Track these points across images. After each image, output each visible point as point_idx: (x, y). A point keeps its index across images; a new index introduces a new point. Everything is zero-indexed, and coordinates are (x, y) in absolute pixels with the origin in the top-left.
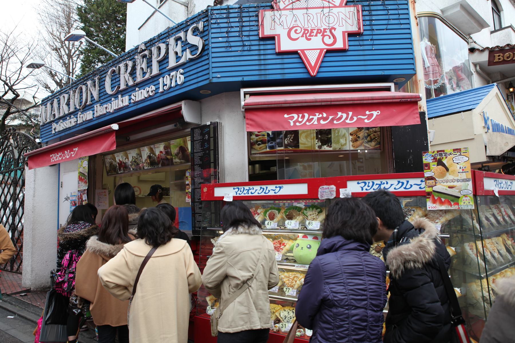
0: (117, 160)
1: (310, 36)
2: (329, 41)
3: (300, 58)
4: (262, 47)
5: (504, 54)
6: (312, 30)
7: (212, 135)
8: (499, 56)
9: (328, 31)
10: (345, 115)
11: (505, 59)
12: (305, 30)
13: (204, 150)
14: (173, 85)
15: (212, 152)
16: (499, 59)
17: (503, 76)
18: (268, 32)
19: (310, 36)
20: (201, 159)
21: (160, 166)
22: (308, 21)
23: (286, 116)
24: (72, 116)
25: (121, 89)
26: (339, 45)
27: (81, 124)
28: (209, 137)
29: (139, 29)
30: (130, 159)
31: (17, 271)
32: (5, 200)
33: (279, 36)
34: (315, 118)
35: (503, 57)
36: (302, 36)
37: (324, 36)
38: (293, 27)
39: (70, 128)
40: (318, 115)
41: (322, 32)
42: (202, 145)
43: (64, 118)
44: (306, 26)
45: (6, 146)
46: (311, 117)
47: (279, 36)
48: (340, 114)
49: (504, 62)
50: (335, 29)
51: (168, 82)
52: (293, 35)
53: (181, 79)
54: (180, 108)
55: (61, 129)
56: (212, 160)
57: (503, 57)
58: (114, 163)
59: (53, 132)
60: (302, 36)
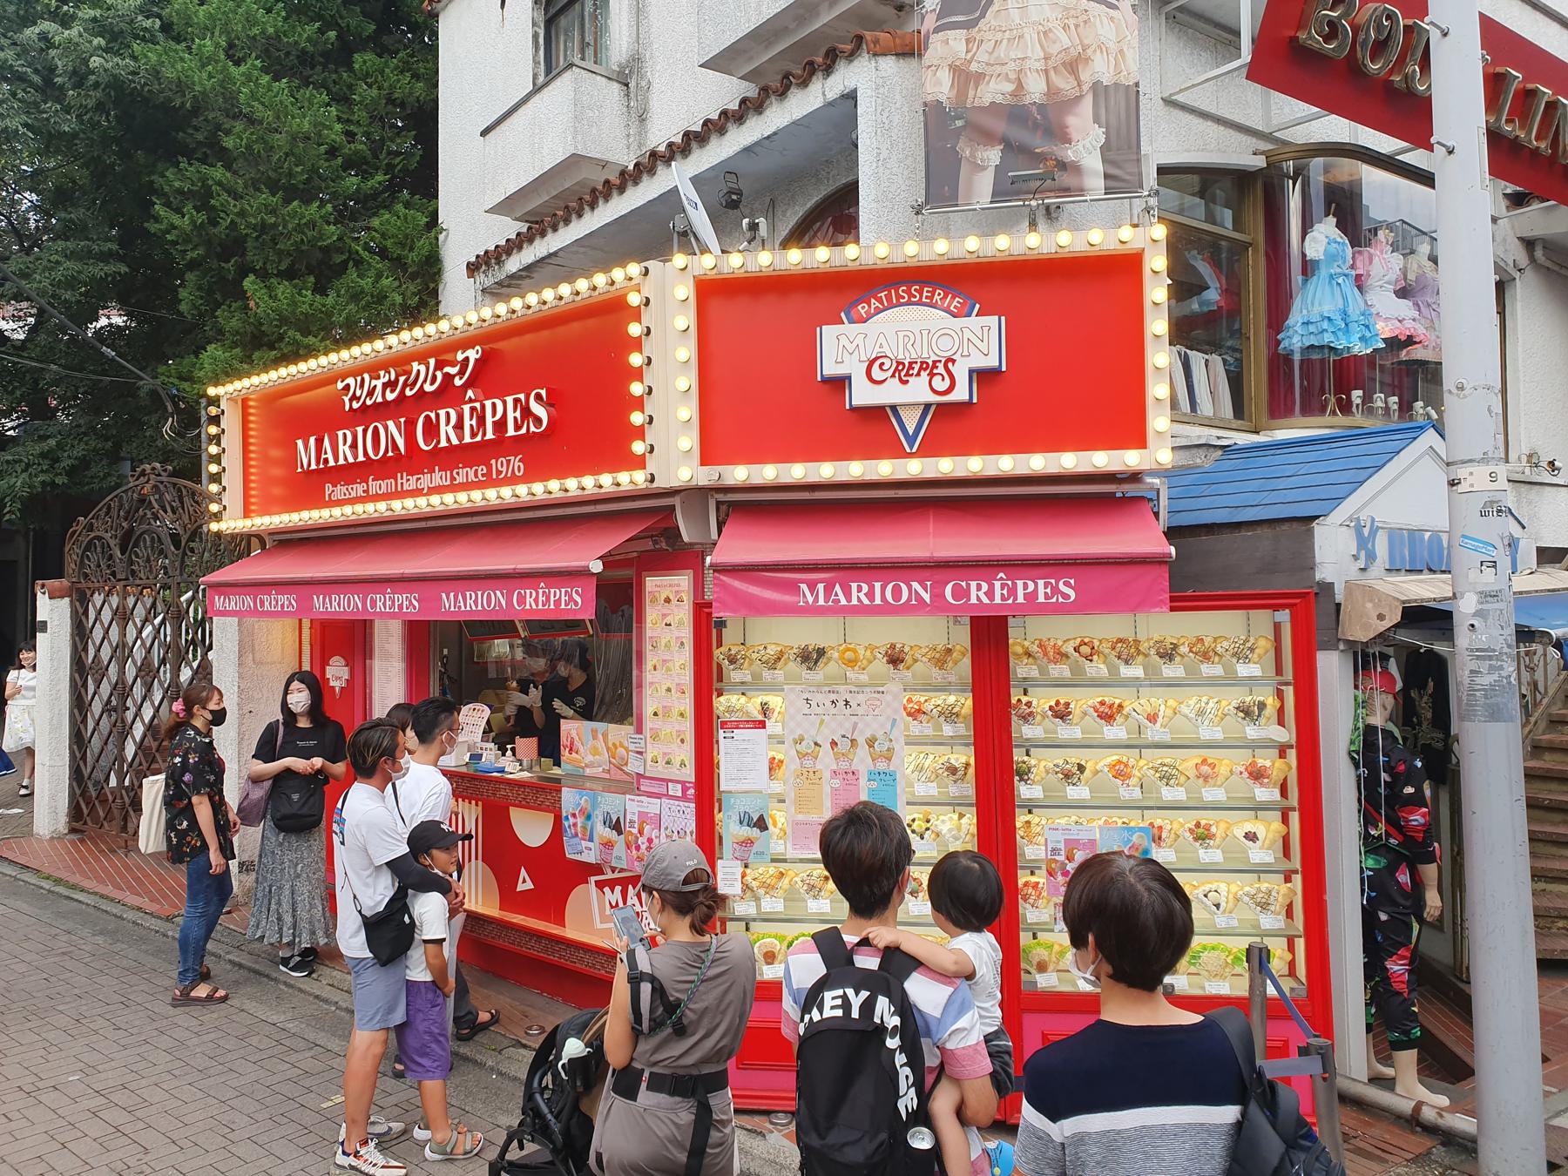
1: (907, 374)
9: (941, 366)
10: (423, 368)
12: (899, 363)
19: (907, 374)
22: (905, 346)
26: (961, 394)
29: (484, 133)
37: (932, 375)
38: (877, 358)
41: (929, 368)
44: (901, 357)
46: (374, 382)
50: (954, 361)
52: (877, 374)
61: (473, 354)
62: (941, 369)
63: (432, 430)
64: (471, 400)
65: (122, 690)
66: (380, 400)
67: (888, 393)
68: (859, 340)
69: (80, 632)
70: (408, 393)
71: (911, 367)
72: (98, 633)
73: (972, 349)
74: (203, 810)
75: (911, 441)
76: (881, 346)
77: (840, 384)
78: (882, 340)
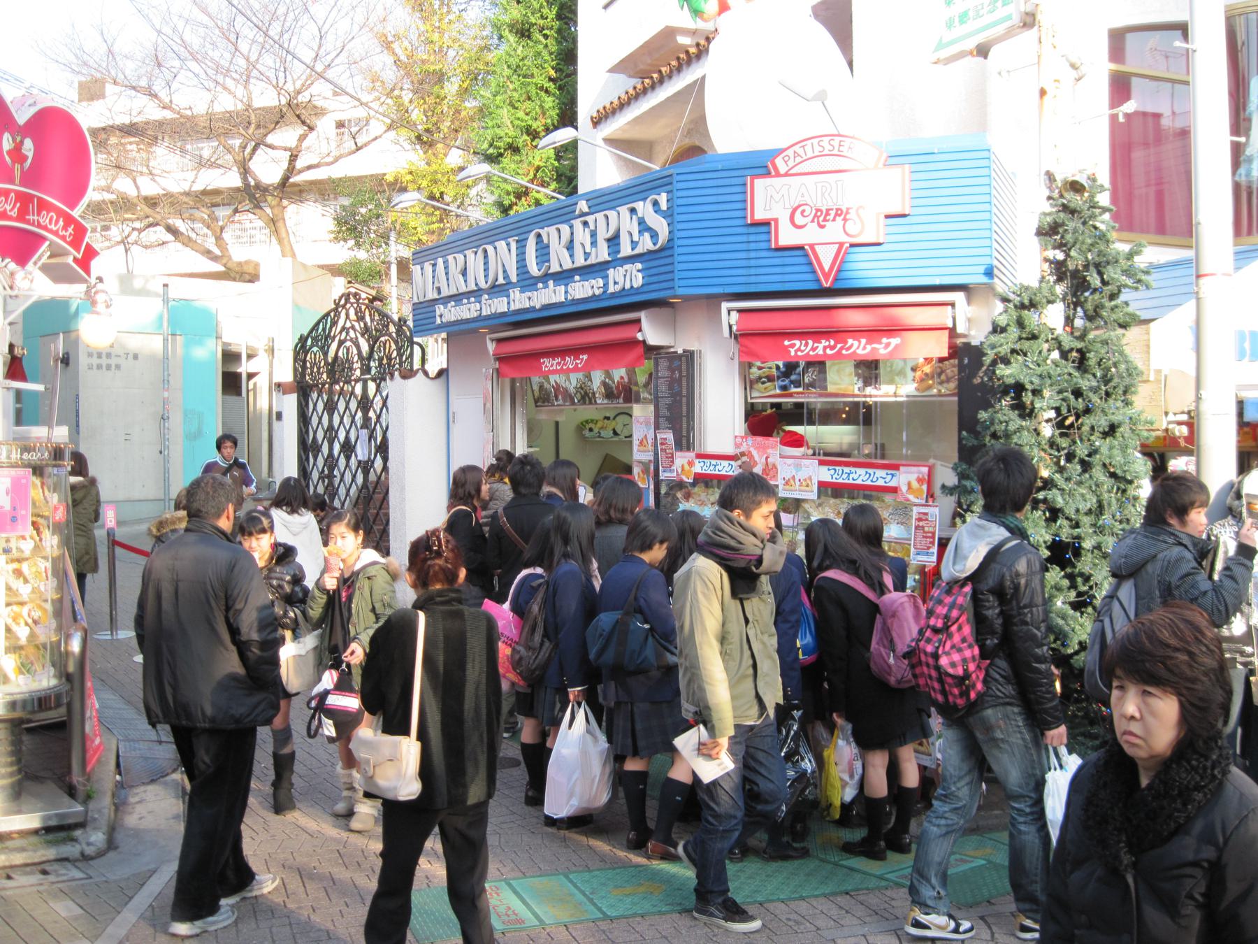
0: (553, 383)
1: (825, 220)
3: (807, 255)
4: (752, 238)
6: (828, 210)
7: (684, 373)
10: (856, 343)
12: (817, 210)
13: (673, 395)
14: (628, 286)
15: (684, 400)
18: (760, 215)
19: (825, 220)
20: (669, 409)
21: (621, 400)
22: (823, 195)
23: (786, 343)
24: (472, 299)
25: (551, 271)
27: (488, 318)
28: (681, 376)
30: (574, 383)
32: (347, 438)
33: (776, 220)
34: (821, 346)
36: (813, 221)
39: (468, 321)
40: (824, 343)
42: (670, 387)
43: (457, 298)
44: (819, 205)
45: (343, 328)
47: (776, 220)
48: (850, 341)
51: (620, 279)
52: (799, 220)
53: (638, 280)
55: (453, 319)
56: (684, 413)
58: (546, 385)
59: (438, 321)
60: (813, 221)
63: (543, 251)
64: (583, 214)
65: (331, 462)
69: (304, 419)
71: (828, 214)
72: (315, 420)
74: (439, 599)
76: (803, 196)
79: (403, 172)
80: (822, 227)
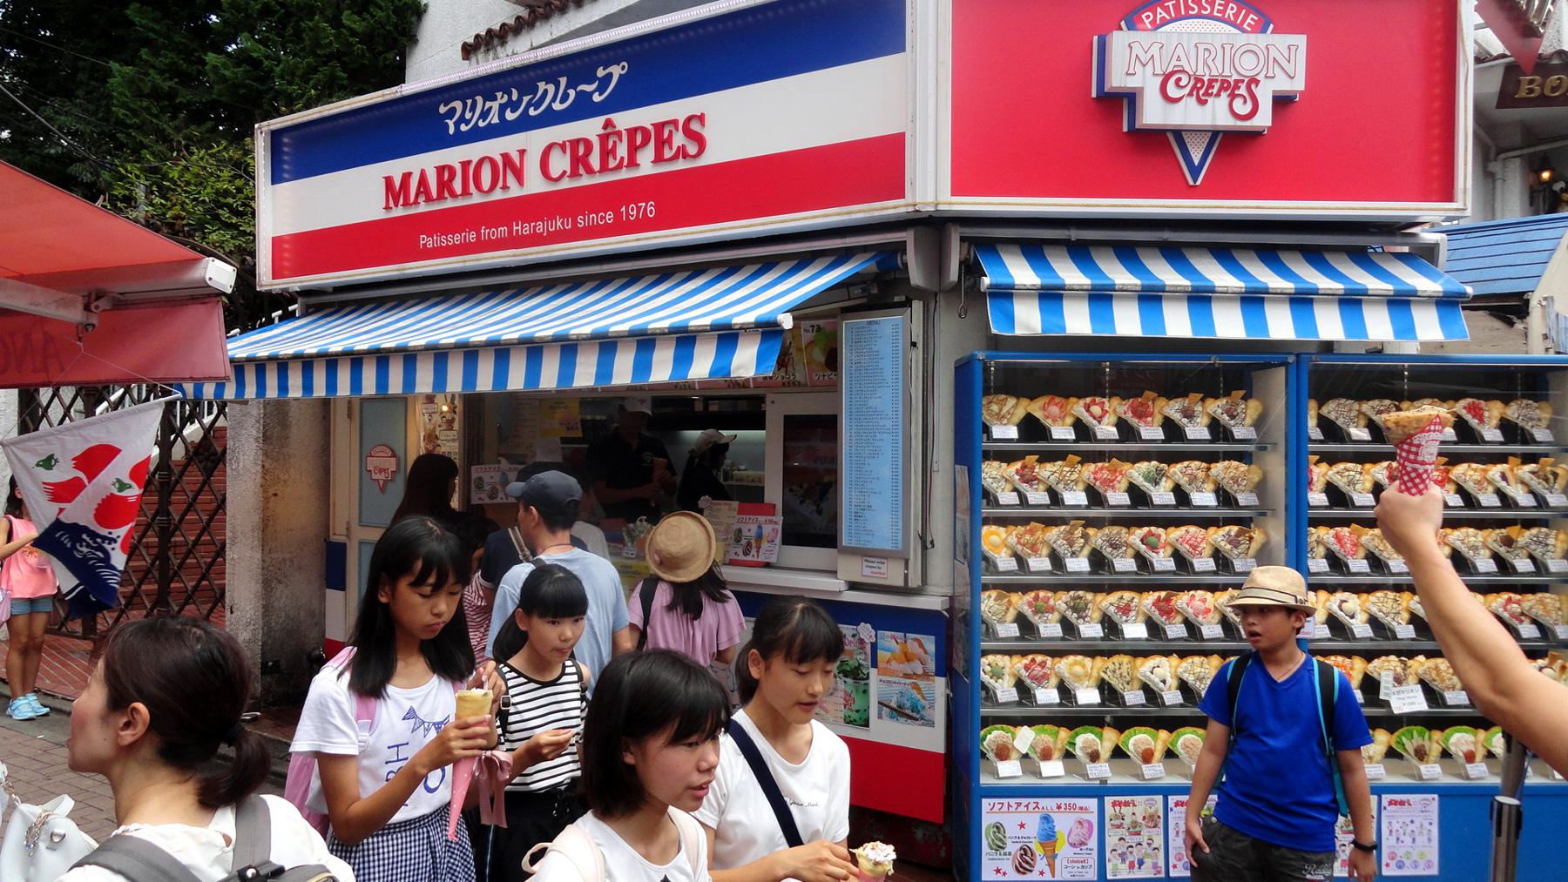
1: (1206, 94)
2: (1242, 108)
5: (1546, 76)
8: (1531, 82)
9: (1243, 86)
10: (551, 88)
11: (1547, 92)
16: (1531, 91)
17: (1531, 135)
18: (1117, 80)
19: (1206, 94)
22: (1205, 63)
26: (1264, 119)
31: (1411, 589)
35: (1542, 86)
36: (1190, 94)
37: (1233, 96)
38: (1173, 73)
41: (1229, 88)
46: (488, 104)
49: (1543, 101)
50: (1257, 82)
52: (1172, 91)
54: (901, 247)
57: (1542, 86)
61: (617, 71)
62: (1243, 90)
66: (496, 120)
67: (1188, 114)
68: (1155, 50)
70: (532, 112)
71: (1210, 86)
73: (1278, 71)
75: (1195, 172)
76: (1179, 59)
77: (1130, 99)
78: (1180, 51)
79: (908, 704)
80: (1202, 102)
